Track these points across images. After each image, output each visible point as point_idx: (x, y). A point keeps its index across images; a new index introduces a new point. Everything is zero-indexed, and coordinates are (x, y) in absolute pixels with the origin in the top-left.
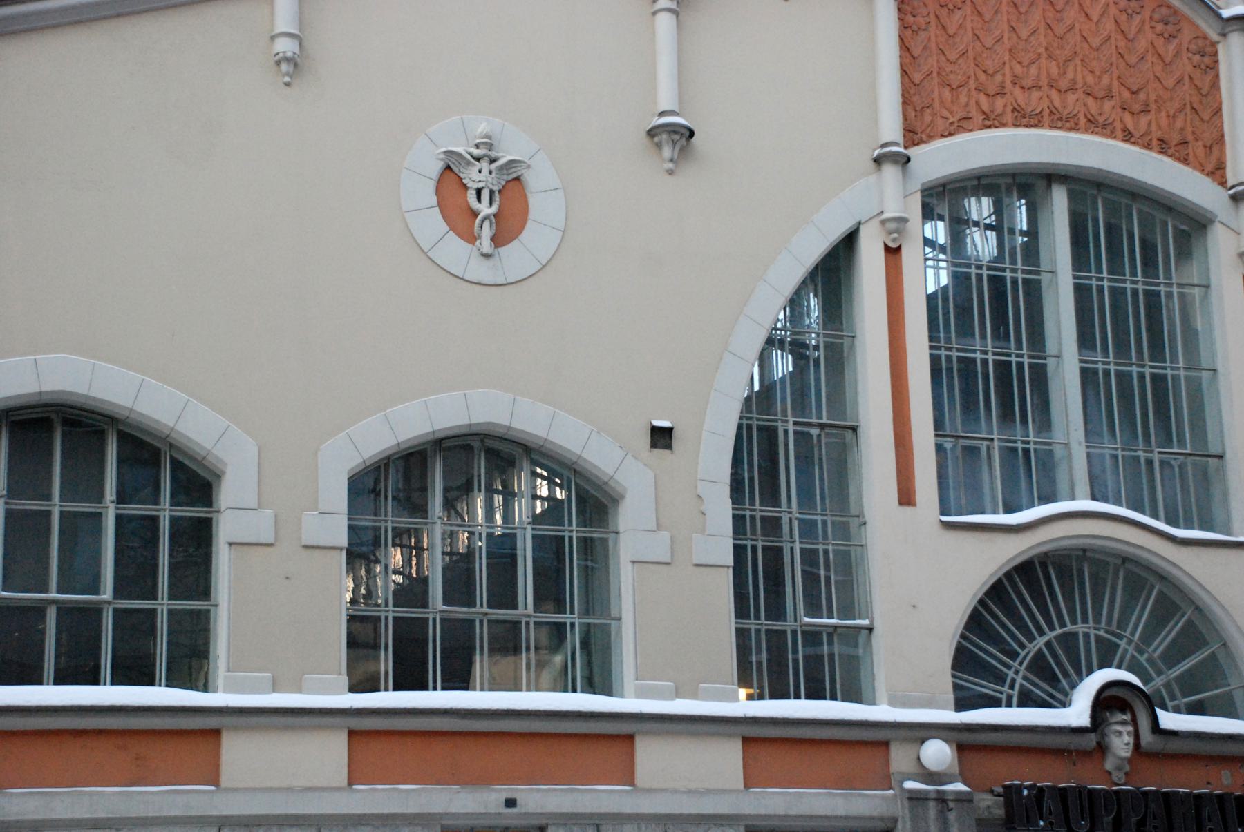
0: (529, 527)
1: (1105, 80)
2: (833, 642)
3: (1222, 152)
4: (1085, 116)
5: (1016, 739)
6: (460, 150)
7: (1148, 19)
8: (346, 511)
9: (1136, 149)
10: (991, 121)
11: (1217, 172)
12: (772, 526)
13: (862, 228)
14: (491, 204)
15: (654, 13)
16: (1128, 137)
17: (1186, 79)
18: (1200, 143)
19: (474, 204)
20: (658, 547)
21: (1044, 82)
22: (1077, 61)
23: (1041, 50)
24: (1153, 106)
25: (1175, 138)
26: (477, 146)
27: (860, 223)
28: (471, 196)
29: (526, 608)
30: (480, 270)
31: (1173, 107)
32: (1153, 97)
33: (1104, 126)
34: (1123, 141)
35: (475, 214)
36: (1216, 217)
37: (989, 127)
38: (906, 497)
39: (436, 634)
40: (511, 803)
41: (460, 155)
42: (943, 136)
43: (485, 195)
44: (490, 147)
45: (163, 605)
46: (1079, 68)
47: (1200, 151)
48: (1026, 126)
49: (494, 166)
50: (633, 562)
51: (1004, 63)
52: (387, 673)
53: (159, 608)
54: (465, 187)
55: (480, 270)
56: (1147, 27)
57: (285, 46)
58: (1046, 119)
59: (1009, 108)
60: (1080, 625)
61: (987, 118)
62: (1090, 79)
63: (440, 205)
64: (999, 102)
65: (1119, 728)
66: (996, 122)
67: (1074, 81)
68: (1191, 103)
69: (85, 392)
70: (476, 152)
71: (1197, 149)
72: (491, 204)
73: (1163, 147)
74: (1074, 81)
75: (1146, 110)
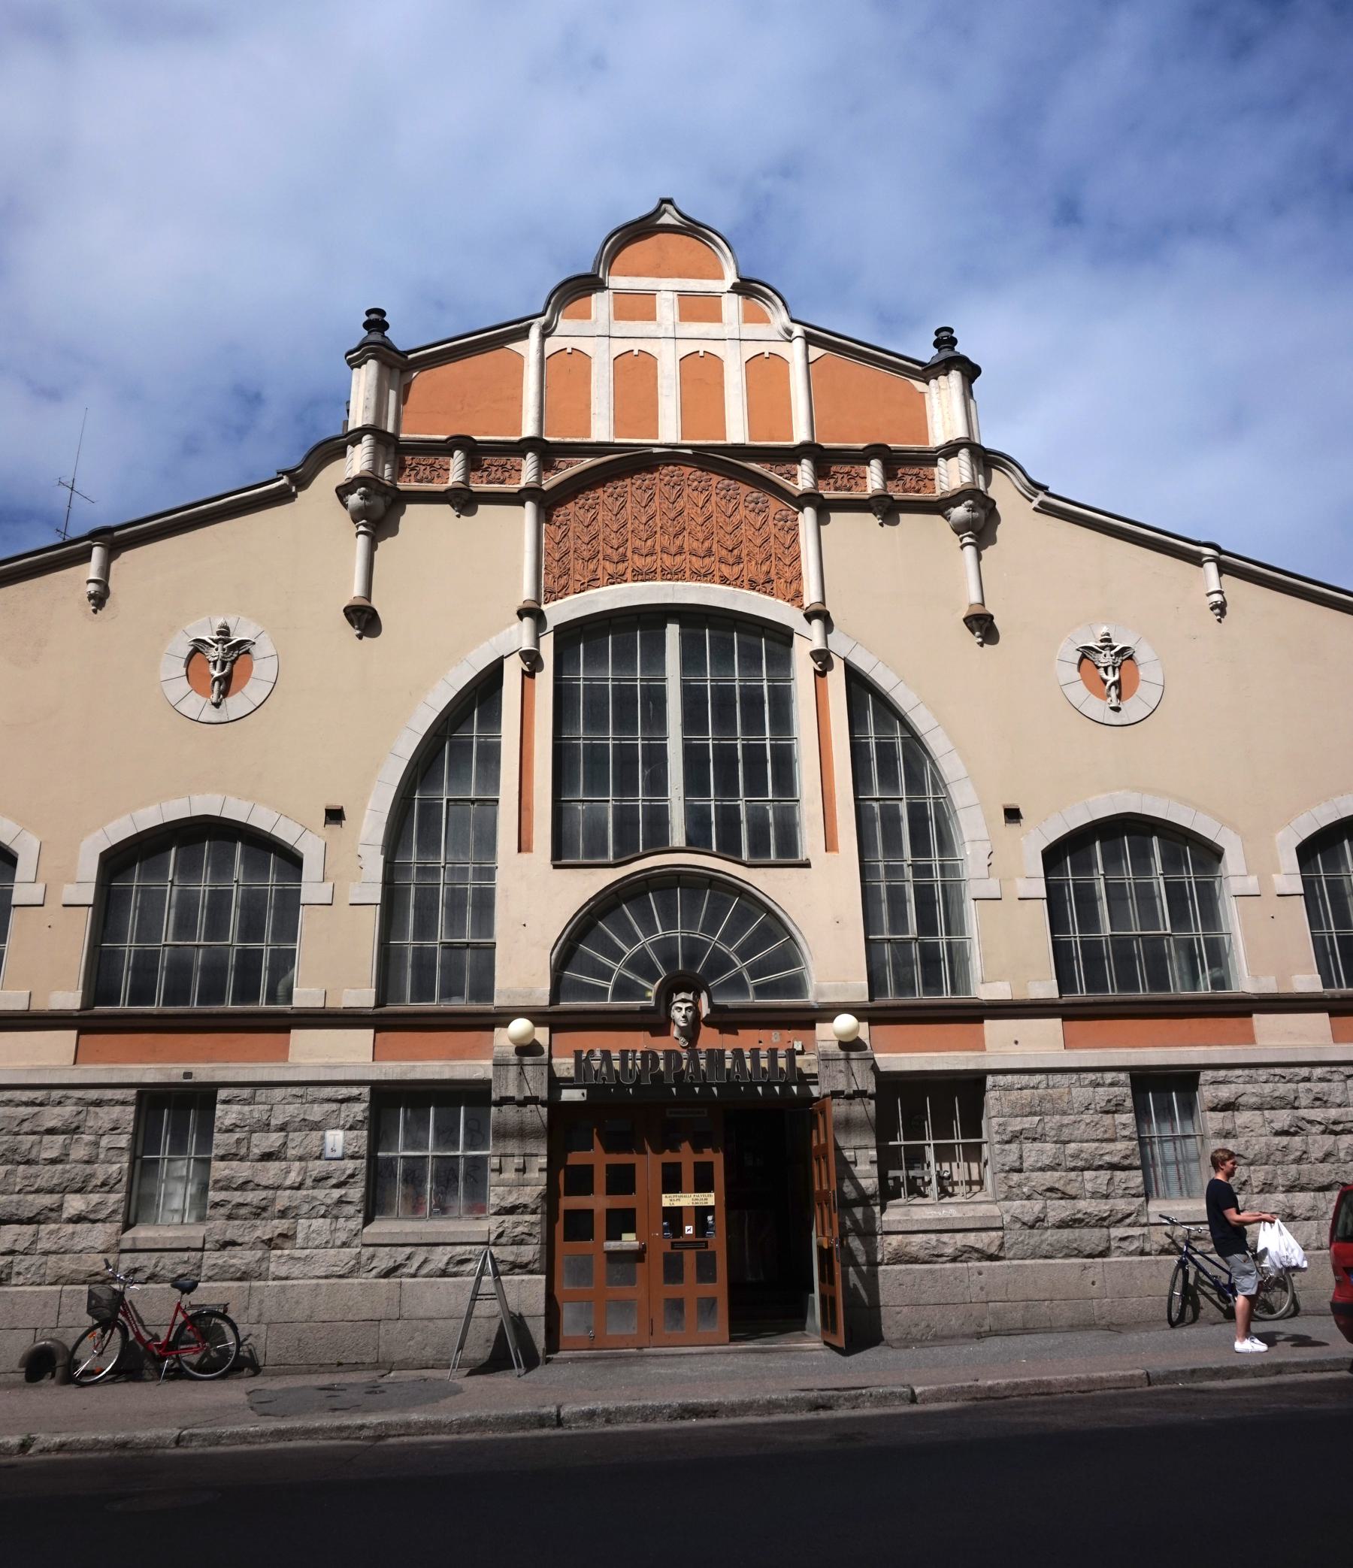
0: (1161, 878)
1: (707, 544)
2: (136, 970)
3: (800, 585)
4: (690, 569)
5: (603, 1019)
6: (206, 638)
7: (742, 501)
8: (1298, 871)
9: (731, 588)
10: (615, 579)
11: (796, 597)
12: (927, 870)
13: (505, 661)
14: (1114, 674)
15: (962, 547)
16: (724, 581)
17: (772, 538)
18: (782, 580)
19: (1105, 676)
20: (1251, 884)
21: (658, 548)
22: (686, 533)
23: (658, 529)
24: (745, 559)
25: (761, 579)
26: (1102, 641)
27: (502, 658)
28: (1102, 671)
29: (1166, 930)
30: (211, 714)
31: (760, 557)
32: (745, 552)
33: (705, 576)
34: (720, 584)
35: (1105, 682)
36: (793, 630)
37: (613, 583)
38: (523, 845)
39: (1107, 949)
40: (188, 1075)
41: (204, 641)
42: (575, 593)
43: (1110, 670)
44: (1109, 640)
45: (942, 939)
46: (686, 539)
47: (783, 586)
48: (642, 581)
49: (1113, 652)
50: (975, 900)
51: (627, 541)
52: (1203, 971)
53: (940, 941)
54: (1098, 668)
55: (211, 714)
56: (741, 507)
57: (1217, 598)
58: (659, 575)
59: (629, 570)
60: (238, 945)
61: (612, 577)
62: (695, 544)
63: (187, 675)
64: (621, 567)
65: (679, 1005)
66: (619, 580)
67: (681, 547)
68: (776, 554)
69: (244, 821)
70: (1103, 644)
71: (779, 584)
72: (1114, 674)
73: (753, 585)
74: (681, 547)
75: (739, 560)
